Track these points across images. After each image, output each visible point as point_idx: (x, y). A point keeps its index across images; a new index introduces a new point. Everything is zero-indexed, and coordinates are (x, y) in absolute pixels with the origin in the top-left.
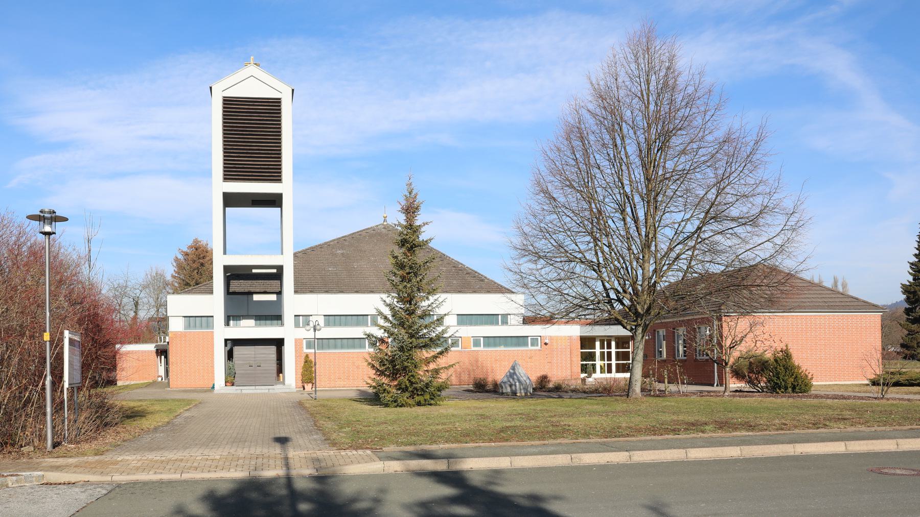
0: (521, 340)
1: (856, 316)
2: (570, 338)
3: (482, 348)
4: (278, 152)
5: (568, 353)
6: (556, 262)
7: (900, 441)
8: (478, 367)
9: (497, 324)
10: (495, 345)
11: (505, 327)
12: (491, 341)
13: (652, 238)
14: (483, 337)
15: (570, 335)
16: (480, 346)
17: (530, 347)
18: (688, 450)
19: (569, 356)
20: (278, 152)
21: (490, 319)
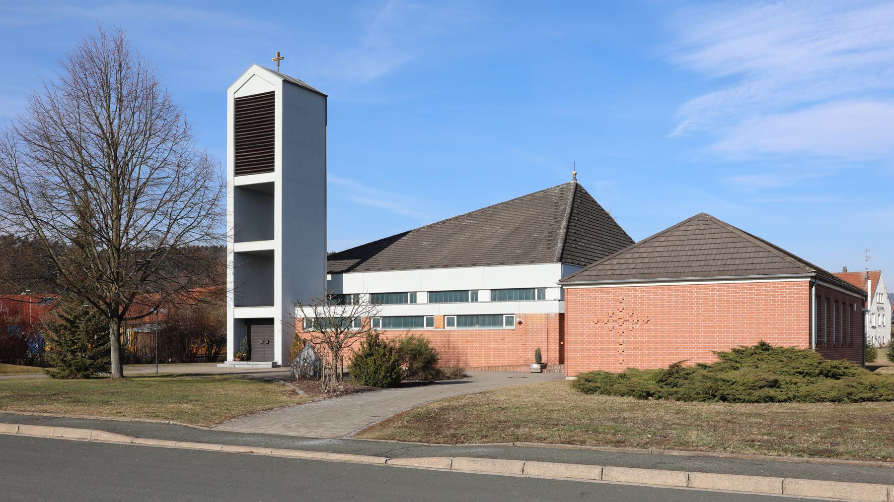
0: (494, 319)
1: (575, 290)
2: (548, 316)
3: (455, 327)
4: (238, 172)
5: (545, 334)
6: (60, 222)
7: (777, 492)
8: (449, 349)
9: (467, 300)
10: (472, 324)
11: (475, 304)
12: (466, 320)
13: (18, 192)
14: (457, 315)
15: (547, 312)
16: (454, 325)
17: (505, 327)
18: (788, 480)
19: (545, 337)
20: (238, 172)
21: (459, 296)
